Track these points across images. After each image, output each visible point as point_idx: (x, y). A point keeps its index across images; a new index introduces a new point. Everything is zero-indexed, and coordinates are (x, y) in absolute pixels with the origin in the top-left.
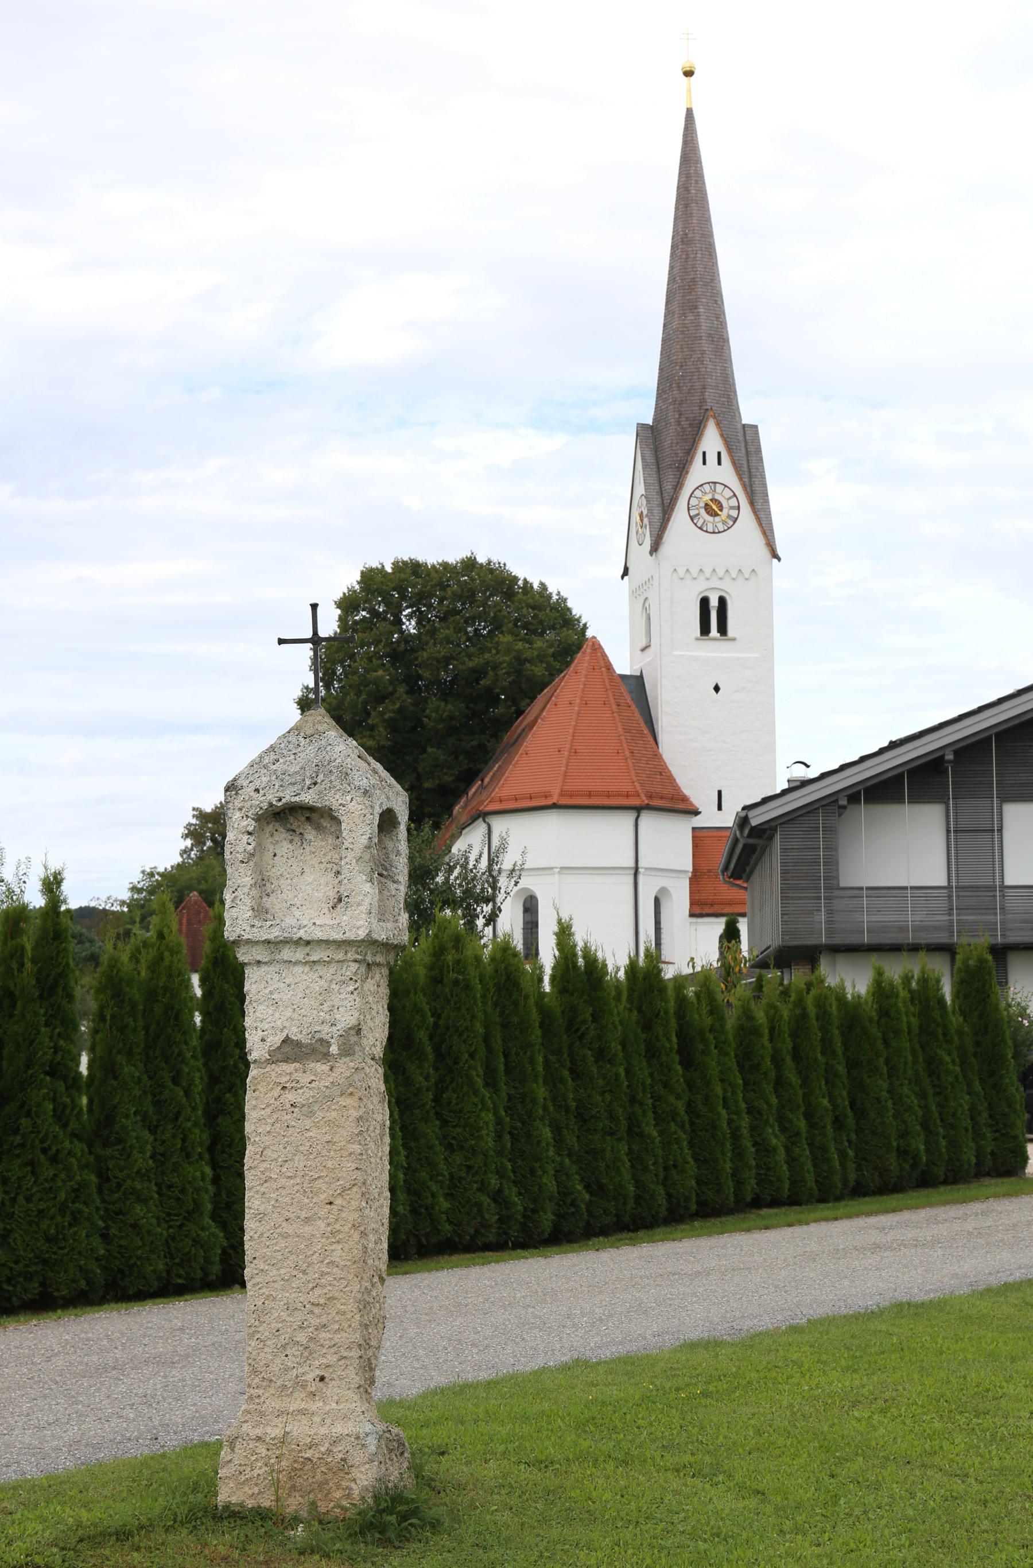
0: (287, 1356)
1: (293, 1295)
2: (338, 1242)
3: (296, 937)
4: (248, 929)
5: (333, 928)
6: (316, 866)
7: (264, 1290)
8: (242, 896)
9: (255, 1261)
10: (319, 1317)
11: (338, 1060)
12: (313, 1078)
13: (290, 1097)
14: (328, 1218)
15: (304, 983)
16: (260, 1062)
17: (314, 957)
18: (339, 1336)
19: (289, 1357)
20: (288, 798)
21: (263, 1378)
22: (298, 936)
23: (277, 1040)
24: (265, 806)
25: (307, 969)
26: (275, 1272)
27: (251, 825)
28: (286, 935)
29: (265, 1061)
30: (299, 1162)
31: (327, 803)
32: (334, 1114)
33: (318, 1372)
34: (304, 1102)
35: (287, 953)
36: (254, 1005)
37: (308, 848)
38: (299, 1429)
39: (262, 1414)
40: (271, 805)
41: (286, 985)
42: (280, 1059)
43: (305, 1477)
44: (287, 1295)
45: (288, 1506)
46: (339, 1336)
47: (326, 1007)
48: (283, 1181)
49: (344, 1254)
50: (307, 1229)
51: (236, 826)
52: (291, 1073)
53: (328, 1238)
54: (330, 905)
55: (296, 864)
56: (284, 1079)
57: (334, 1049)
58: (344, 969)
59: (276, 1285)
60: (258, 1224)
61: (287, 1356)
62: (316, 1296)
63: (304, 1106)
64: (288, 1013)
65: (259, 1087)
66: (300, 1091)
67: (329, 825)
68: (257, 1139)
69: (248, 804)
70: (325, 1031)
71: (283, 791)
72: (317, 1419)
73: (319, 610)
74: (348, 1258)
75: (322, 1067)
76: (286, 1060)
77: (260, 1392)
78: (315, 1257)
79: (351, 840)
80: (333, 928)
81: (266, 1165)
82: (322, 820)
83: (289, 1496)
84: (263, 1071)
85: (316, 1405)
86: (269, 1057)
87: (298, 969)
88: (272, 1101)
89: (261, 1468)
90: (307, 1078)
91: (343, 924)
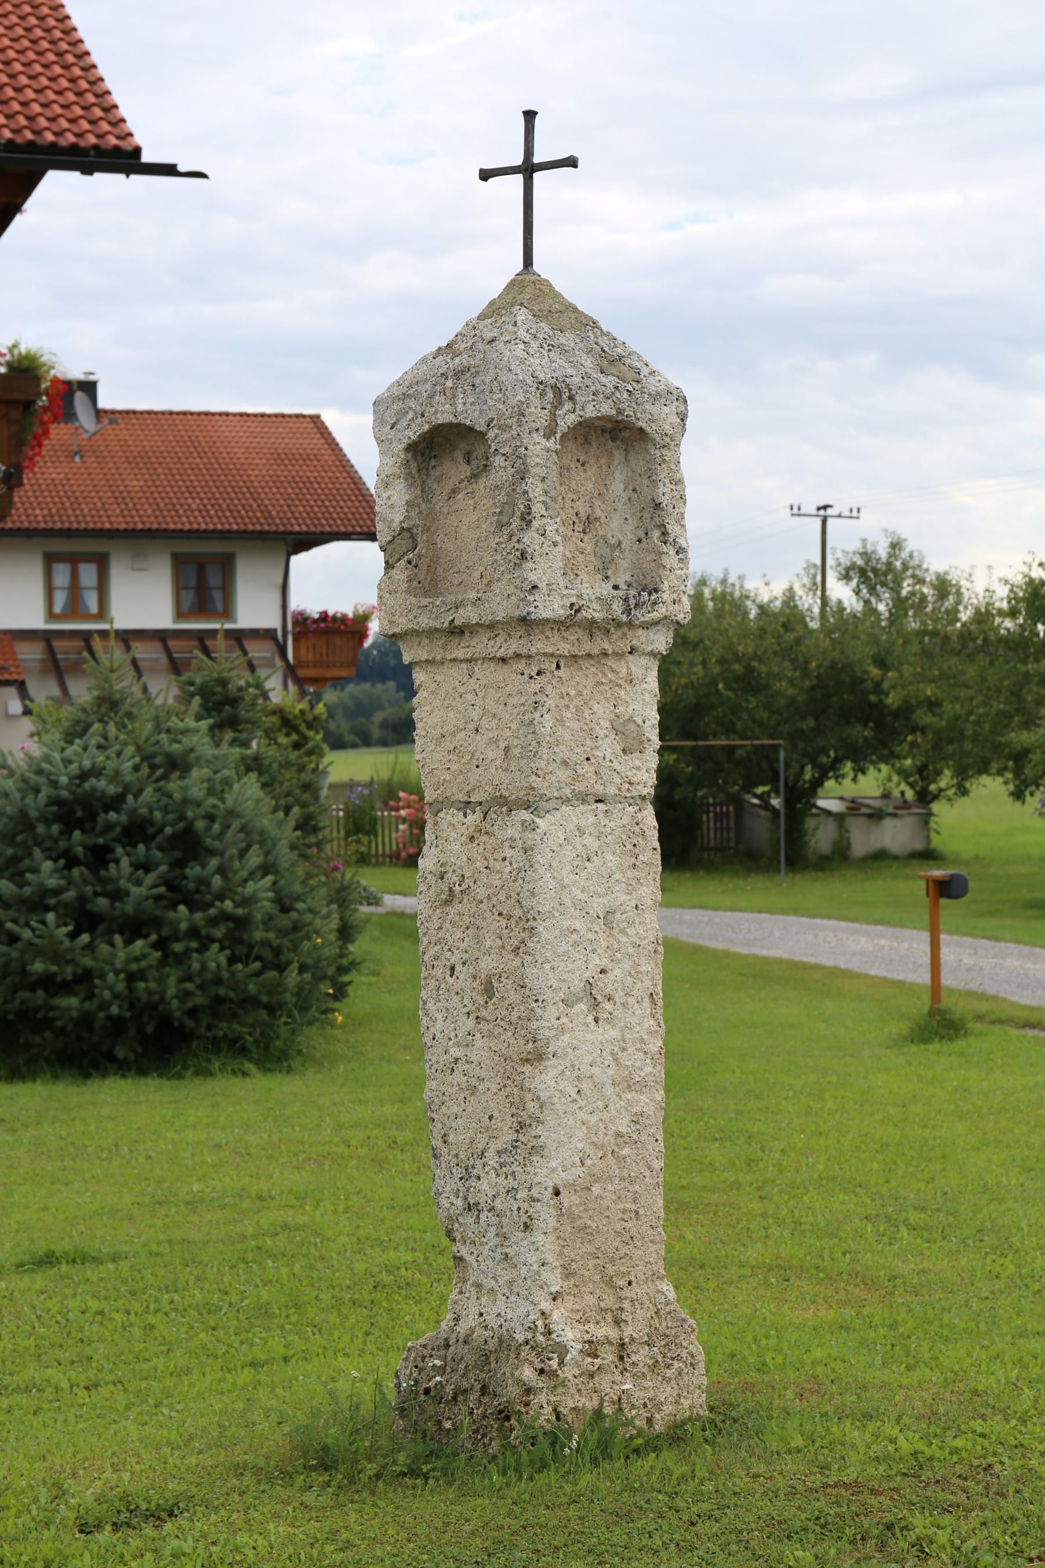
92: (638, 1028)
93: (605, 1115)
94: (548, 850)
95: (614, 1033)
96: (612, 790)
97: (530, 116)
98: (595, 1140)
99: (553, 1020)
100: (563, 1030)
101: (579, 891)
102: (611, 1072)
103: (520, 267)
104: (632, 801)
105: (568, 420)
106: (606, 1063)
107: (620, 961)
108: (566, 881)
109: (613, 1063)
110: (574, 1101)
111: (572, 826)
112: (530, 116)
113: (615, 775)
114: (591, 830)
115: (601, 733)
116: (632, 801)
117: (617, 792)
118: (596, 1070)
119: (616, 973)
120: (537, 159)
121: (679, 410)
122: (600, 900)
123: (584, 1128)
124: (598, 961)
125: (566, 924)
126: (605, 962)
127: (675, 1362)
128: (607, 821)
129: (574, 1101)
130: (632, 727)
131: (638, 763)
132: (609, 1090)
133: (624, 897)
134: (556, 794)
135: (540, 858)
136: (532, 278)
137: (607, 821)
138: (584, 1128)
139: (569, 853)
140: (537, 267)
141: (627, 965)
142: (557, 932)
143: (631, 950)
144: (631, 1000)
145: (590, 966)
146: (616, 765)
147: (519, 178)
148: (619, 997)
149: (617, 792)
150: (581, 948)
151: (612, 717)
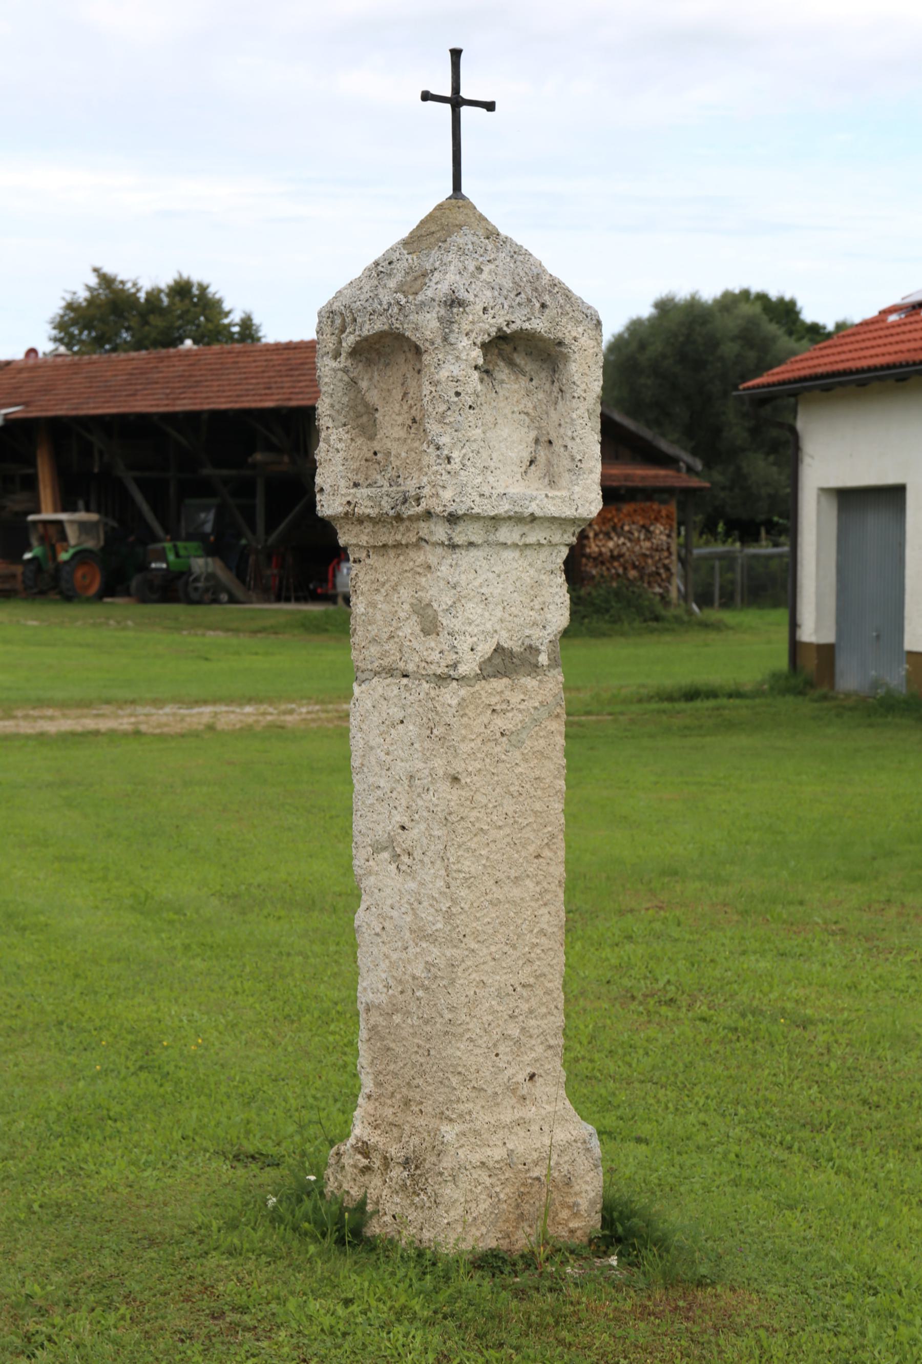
0: (497, 1055)
1: (504, 977)
2: (545, 905)
3: (527, 512)
4: (477, 499)
5: (564, 501)
6: (510, 416)
7: (474, 975)
8: (471, 455)
9: (465, 940)
10: (528, 1001)
11: (547, 673)
12: (522, 697)
13: (500, 723)
14: (537, 875)
15: (514, 572)
16: (469, 679)
17: (531, 539)
18: (546, 1022)
19: (501, 1056)
20: (518, 323)
21: (474, 1087)
22: (530, 510)
23: (486, 649)
24: (493, 332)
25: (517, 554)
26: (485, 951)
27: (477, 355)
28: (517, 509)
29: (474, 677)
30: (509, 806)
31: (560, 335)
32: (542, 742)
33: (529, 1070)
34: (514, 729)
35: (506, 534)
36: (463, 601)
37: (501, 393)
38: (519, 1143)
39: (477, 1133)
40: (500, 329)
41: (495, 575)
42: (491, 674)
43: (532, 1202)
44: (498, 978)
45: (517, 1241)
46: (546, 1022)
47: (537, 605)
48: (494, 833)
49: (551, 919)
50: (516, 892)
51: (463, 356)
52: (502, 692)
53: (538, 900)
54: (523, 470)
55: (490, 412)
56: (493, 700)
57: (543, 659)
58: (554, 554)
59: (486, 967)
60: (467, 891)
61: (497, 1055)
62: (525, 975)
63: (512, 733)
64: (499, 613)
65: (467, 712)
66: (510, 715)
67: (523, 362)
68: (468, 780)
69: (477, 327)
70: (536, 633)
71: (512, 313)
72: (535, 1128)
73: (463, 58)
74: (555, 923)
75: (530, 682)
76: (498, 674)
77: (470, 1106)
78: (524, 926)
79: (583, 386)
80: (564, 501)
81: (475, 813)
82: (515, 355)
83: (517, 1228)
84: (472, 690)
85: (530, 1112)
86: (479, 672)
87: (508, 555)
88: (482, 729)
89: (485, 1200)
90: (515, 698)
91: (576, 497)
92: (431, 886)
93: (404, 955)
94: (358, 714)
95: (412, 885)
96: (411, 667)
97: (456, 54)
98: (396, 975)
99: (363, 861)
100: (370, 873)
101: (383, 753)
102: (408, 919)
103: (450, 192)
104: (428, 679)
105: (349, 340)
106: (403, 910)
107: (418, 823)
108: (372, 743)
109: (410, 911)
110: (377, 935)
111: (377, 696)
112: (456, 54)
113: (415, 654)
114: (395, 700)
115: (402, 615)
116: (428, 679)
117: (415, 669)
118: (394, 913)
119: (414, 833)
120: (448, 93)
121: (440, 314)
122: (403, 764)
123: (387, 961)
124: (399, 818)
125: (371, 780)
126: (405, 820)
127: (422, 1193)
128: (408, 694)
129: (377, 935)
130: (430, 612)
131: (433, 644)
132: (407, 935)
133: (421, 765)
134: (369, 667)
135: (354, 722)
136: (461, 203)
137: (408, 694)
138: (387, 961)
139: (375, 719)
140: (465, 190)
141: (423, 826)
142: (366, 786)
143: (425, 814)
144: (426, 859)
145: (393, 821)
146: (415, 644)
147: (465, 110)
148: (417, 854)
149: (415, 669)
150: (385, 804)
151: (414, 601)
